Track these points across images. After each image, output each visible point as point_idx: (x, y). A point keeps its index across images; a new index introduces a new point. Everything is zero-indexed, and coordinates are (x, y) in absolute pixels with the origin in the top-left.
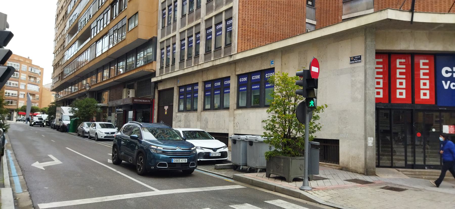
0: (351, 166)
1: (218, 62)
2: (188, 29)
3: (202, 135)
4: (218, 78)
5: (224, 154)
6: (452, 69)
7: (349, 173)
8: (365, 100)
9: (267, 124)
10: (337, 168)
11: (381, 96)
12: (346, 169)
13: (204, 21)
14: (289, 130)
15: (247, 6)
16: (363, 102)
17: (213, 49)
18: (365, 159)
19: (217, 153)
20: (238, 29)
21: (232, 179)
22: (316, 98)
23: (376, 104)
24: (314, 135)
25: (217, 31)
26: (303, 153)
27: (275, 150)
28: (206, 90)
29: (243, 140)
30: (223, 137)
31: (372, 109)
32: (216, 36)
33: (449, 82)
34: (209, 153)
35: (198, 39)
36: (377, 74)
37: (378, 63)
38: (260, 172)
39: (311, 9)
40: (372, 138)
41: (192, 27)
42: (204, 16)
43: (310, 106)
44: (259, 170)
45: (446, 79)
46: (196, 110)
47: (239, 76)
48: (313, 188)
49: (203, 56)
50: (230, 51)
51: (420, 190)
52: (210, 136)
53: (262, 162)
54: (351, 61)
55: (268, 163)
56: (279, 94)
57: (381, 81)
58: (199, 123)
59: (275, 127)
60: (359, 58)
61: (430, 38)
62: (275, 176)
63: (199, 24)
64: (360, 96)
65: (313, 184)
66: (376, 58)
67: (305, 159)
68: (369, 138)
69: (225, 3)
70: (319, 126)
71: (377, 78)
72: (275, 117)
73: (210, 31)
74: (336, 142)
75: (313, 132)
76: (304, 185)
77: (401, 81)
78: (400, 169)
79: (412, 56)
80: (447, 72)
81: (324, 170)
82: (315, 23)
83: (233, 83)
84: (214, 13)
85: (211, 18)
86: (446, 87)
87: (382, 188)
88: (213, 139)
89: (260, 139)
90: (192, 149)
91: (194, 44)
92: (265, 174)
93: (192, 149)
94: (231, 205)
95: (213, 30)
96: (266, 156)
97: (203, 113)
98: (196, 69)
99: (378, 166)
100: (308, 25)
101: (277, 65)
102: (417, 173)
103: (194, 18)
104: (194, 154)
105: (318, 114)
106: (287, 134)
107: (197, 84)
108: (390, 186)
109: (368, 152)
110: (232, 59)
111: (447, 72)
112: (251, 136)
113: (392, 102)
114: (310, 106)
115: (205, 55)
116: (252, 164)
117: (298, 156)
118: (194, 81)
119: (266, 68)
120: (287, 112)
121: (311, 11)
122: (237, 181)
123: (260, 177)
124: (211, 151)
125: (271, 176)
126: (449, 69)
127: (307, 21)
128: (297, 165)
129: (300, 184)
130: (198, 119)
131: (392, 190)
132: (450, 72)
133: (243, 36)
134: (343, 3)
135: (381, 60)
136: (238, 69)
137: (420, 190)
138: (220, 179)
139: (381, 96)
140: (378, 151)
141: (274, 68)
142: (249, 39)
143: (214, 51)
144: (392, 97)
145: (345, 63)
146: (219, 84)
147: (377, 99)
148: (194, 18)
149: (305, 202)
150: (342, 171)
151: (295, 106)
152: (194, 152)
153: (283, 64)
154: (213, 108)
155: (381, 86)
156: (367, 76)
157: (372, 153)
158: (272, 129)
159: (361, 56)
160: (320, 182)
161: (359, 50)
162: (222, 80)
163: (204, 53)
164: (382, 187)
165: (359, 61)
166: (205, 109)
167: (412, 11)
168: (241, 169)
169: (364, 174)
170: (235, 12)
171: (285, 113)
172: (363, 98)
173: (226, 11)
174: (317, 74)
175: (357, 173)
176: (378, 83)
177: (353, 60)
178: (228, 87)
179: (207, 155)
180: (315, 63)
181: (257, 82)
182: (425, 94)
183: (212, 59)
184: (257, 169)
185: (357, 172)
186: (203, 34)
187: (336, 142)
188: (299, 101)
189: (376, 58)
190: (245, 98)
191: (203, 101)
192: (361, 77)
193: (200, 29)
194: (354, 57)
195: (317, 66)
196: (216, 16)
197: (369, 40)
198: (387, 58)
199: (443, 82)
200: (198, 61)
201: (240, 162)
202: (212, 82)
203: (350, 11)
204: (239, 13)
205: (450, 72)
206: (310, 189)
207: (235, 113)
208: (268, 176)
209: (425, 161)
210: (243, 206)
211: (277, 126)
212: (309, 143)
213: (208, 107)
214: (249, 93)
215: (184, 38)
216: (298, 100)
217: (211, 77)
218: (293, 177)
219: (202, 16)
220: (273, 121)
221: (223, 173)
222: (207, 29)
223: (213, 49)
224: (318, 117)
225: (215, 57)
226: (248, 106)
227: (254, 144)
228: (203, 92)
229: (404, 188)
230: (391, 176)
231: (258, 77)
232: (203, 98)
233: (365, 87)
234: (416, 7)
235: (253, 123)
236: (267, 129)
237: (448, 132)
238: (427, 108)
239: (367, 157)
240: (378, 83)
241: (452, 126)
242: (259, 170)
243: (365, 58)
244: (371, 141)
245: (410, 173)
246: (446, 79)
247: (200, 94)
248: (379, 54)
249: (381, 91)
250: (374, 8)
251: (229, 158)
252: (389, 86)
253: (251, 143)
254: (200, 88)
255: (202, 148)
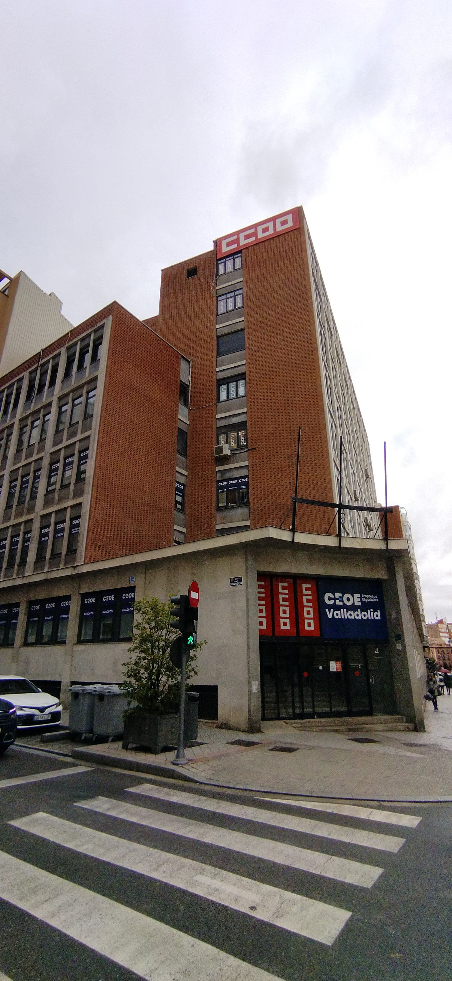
0: (233, 722)
1: (54, 575)
2: (13, 526)
3: (22, 687)
4: (53, 596)
5: (56, 716)
6: (334, 595)
7: (230, 732)
8: (248, 633)
9: (129, 669)
10: (215, 725)
11: (264, 627)
12: (226, 726)
13: (39, 518)
14: (158, 677)
15: (101, 503)
16: (245, 635)
17: (48, 556)
18: (249, 711)
19: (46, 716)
20: (88, 532)
21: (70, 756)
22: (196, 633)
23: (261, 637)
24: (190, 682)
25: (56, 531)
26: (176, 709)
27: (137, 706)
28: (30, 614)
29: (90, 693)
30: (52, 687)
31: (255, 644)
32: (55, 538)
33: (332, 610)
34: (32, 716)
35: (26, 540)
36: (259, 600)
37: (260, 587)
38: (113, 741)
39: (180, 513)
40: (257, 682)
41: (20, 524)
42: (40, 510)
43: (189, 643)
44: (111, 739)
45: (330, 607)
46: (12, 645)
47: (84, 596)
48: (189, 760)
49: (32, 564)
50: (74, 560)
51: (314, 748)
52: (34, 686)
53: (117, 724)
54: (231, 582)
55: (126, 727)
56: (147, 626)
57: (264, 608)
58: (14, 666)
59: (139, 672)
60: (240, 581)
61: (311, 559)
62: (134, 746)
63: (32, 520)
64: (241, 627)
65: (189, 753)
66: (258, 580)
67: (180, 717)
68: (253, 682)
69: (71, 496)
70: (196, 670)
71: (259, 605)
72: (140, 659)
73: (46, 530)
74: (213, 690)
75: (188, 678)
76: (178, 757)
77: (284, 608)
78: (288, 721)
79: (295, 580)
80: (330, 599)
81: (204, 732)
82: (184, 530)
83: (74, 607)
84: (55, 508)
85: (50, 514)
86: (330, 616)
87: (271, 750)
88: (39, 692)
89: (115, 689)
90: (11, 711)
91: (19, 547)
92: (121, 744)
93: (11, 711)
94: (76, 802)
95: (51, 530)
96: (124, 716)
97: (22, 649)
98: (19, 582)
99: (264, 719)
100: (176, 532)
101: (139, 582)
102: (307, 725)
103: (25, 512)
104: (13, 719)
105: (195, 653)
106: (155, 683)
107: (18, 605)
108: (279, 745)
109: (252, 701)
110: (76, 572)
111: (330, 599)
112: (100, 686)
113: (277, 634)
114: (189, 643)
115: (35, 562)
116: (100, 729)
117: (168, 713)
118: (14, 600)
119: (124, 586)
120: (156, 651)
121: (180, 516)
122: (78, 759)
123: (115, 749)
124: (36, 712)
125: (130, 746)
126: (332, 596)
127: (175, 527)
128: (168, 727)
129: (171, 755)
130: (13, 659)
131: (283, 751)
132: (332, 599)
133: (92, 541)
134: (217, 510)
135: (263, 583)
136: (83, 586)
137: (314, 748)
138: (50, 759)
139: (264, 627)
140: (263, 697)
141: (135, 586)
142: (101, 546)
143: (50, 559)
144: (276, 629)
145: (224, 585)
146: (53, 605)
147: (260, 630)
148: (25, 512)
149: (180, 782)
150: (221, 730)
151: (166, 643)
152: (13, 716)
153: (147, 582)
154: (39, 642)
155: (264, 614)
156: (249, 602)
157: (256, 702)
158: (135, 676)
159: (241, 578)
160: (196, 749)
161: (240, 572)
162: (58, 600)
163: (34, 560)
164: (271, 748)
165: (240, 583)
166: (26, 644)
167: (293, 531)
168: (83, 738)
169: (248, 732)
170: (86, 510)
171: (153, 652)
172: (246, 629)
173: (72, 507)
174: (197, 600)
175: (240, 731)
176: (261, 611)
177: (233, 582)
178: (67, 610)
179: (29, 719)
180: (194, 587)
181: (109, 605)
182: (310, 625)
183: (46, 570)
184: (108, 737)
185: (238, 730)
186: (35, 534)
187: (213, 690)
188: (173, 637)
189: (258, 580)
190: (90, 625)
191: (24, 630)
192: (242, 604)
193: (31, 527)
194: (234, 578)
195: (197, 590)
196: (57, 512)
197: (250, 559)
198: (269, 580)
199: (327, 610)
200: (24, 571)
201: (82, 726)
202: (43, 602)
203: (225, 521)
204: (90, 511)
205: (332, 599)
206: (186, 762)
207: (74, 649)
208: (125, 747)
209: (313, 707)
210: (96, 802)
211: (142, 671)
212: (186, 694)
213: (32, 639)
214: (98, 619)
215: (5, 537)
216: (171, 634)
217: (42, 595)
218: (161, 745)
219: (36, 510)
220: (136, 663)
221: (55, 747)
222: (42, 528)
223: (48, 556)
224: (195, 656)
225: (49, 568)
226: (95, 640)
227: (105, 698)
228: (26, 617)
229: (295, 747)
230: (279, 732)
231: (112, 598)
232: (25, 626)
233: (248, 616)
234: (297, 526)
235: (106, 665)
236: (129, 676)
237: (335, 670)
238: (311, 641)
239: (252, 708)
240: (261, 611)
241: (338, 662)
242: (111, 739)
243: (247, 583)
244: (255, 686)
245: (300, 725)
246: (330, 607)
247: (22, 620)
248: (261, 576)
249: (264, 620)
250: (250, 519)
251: (64, 721)
252: (273, 616)
253: (101, 697)
254: (22, 611)
255: (21, 708)
